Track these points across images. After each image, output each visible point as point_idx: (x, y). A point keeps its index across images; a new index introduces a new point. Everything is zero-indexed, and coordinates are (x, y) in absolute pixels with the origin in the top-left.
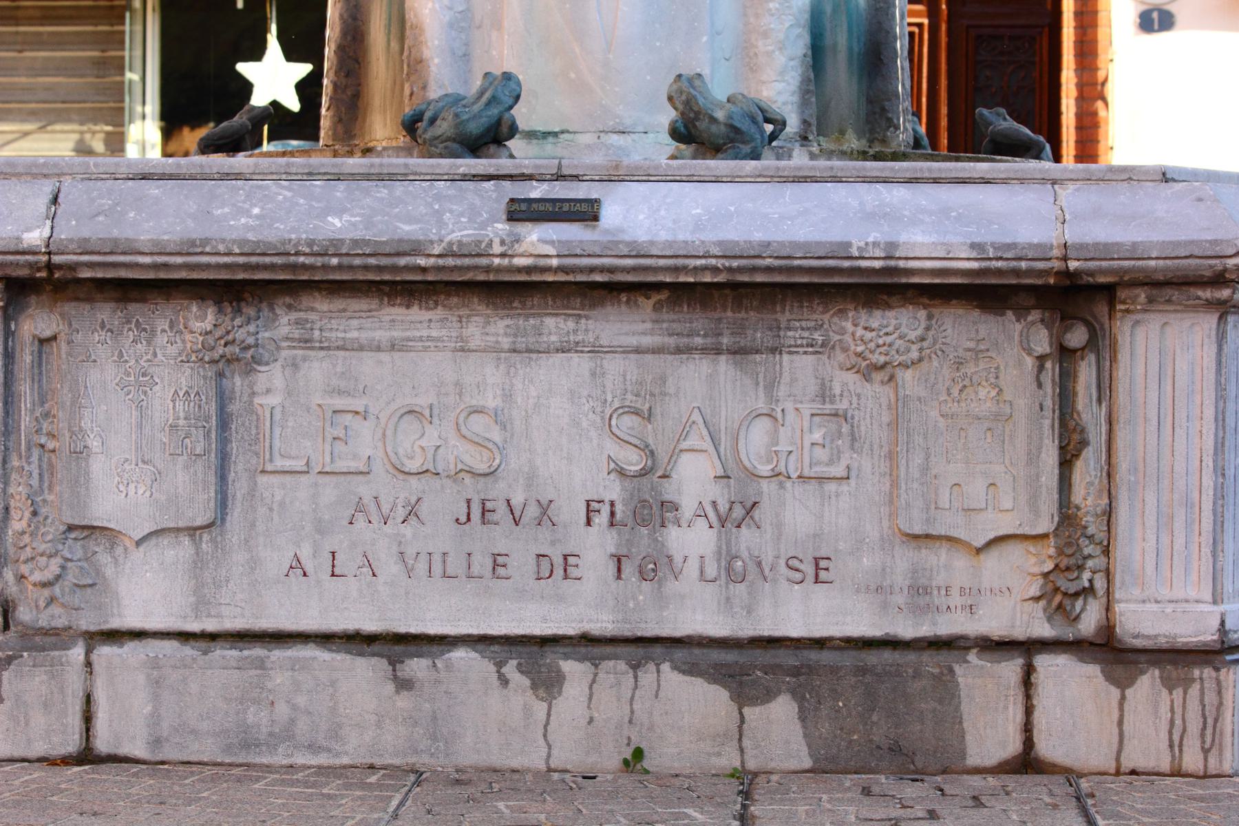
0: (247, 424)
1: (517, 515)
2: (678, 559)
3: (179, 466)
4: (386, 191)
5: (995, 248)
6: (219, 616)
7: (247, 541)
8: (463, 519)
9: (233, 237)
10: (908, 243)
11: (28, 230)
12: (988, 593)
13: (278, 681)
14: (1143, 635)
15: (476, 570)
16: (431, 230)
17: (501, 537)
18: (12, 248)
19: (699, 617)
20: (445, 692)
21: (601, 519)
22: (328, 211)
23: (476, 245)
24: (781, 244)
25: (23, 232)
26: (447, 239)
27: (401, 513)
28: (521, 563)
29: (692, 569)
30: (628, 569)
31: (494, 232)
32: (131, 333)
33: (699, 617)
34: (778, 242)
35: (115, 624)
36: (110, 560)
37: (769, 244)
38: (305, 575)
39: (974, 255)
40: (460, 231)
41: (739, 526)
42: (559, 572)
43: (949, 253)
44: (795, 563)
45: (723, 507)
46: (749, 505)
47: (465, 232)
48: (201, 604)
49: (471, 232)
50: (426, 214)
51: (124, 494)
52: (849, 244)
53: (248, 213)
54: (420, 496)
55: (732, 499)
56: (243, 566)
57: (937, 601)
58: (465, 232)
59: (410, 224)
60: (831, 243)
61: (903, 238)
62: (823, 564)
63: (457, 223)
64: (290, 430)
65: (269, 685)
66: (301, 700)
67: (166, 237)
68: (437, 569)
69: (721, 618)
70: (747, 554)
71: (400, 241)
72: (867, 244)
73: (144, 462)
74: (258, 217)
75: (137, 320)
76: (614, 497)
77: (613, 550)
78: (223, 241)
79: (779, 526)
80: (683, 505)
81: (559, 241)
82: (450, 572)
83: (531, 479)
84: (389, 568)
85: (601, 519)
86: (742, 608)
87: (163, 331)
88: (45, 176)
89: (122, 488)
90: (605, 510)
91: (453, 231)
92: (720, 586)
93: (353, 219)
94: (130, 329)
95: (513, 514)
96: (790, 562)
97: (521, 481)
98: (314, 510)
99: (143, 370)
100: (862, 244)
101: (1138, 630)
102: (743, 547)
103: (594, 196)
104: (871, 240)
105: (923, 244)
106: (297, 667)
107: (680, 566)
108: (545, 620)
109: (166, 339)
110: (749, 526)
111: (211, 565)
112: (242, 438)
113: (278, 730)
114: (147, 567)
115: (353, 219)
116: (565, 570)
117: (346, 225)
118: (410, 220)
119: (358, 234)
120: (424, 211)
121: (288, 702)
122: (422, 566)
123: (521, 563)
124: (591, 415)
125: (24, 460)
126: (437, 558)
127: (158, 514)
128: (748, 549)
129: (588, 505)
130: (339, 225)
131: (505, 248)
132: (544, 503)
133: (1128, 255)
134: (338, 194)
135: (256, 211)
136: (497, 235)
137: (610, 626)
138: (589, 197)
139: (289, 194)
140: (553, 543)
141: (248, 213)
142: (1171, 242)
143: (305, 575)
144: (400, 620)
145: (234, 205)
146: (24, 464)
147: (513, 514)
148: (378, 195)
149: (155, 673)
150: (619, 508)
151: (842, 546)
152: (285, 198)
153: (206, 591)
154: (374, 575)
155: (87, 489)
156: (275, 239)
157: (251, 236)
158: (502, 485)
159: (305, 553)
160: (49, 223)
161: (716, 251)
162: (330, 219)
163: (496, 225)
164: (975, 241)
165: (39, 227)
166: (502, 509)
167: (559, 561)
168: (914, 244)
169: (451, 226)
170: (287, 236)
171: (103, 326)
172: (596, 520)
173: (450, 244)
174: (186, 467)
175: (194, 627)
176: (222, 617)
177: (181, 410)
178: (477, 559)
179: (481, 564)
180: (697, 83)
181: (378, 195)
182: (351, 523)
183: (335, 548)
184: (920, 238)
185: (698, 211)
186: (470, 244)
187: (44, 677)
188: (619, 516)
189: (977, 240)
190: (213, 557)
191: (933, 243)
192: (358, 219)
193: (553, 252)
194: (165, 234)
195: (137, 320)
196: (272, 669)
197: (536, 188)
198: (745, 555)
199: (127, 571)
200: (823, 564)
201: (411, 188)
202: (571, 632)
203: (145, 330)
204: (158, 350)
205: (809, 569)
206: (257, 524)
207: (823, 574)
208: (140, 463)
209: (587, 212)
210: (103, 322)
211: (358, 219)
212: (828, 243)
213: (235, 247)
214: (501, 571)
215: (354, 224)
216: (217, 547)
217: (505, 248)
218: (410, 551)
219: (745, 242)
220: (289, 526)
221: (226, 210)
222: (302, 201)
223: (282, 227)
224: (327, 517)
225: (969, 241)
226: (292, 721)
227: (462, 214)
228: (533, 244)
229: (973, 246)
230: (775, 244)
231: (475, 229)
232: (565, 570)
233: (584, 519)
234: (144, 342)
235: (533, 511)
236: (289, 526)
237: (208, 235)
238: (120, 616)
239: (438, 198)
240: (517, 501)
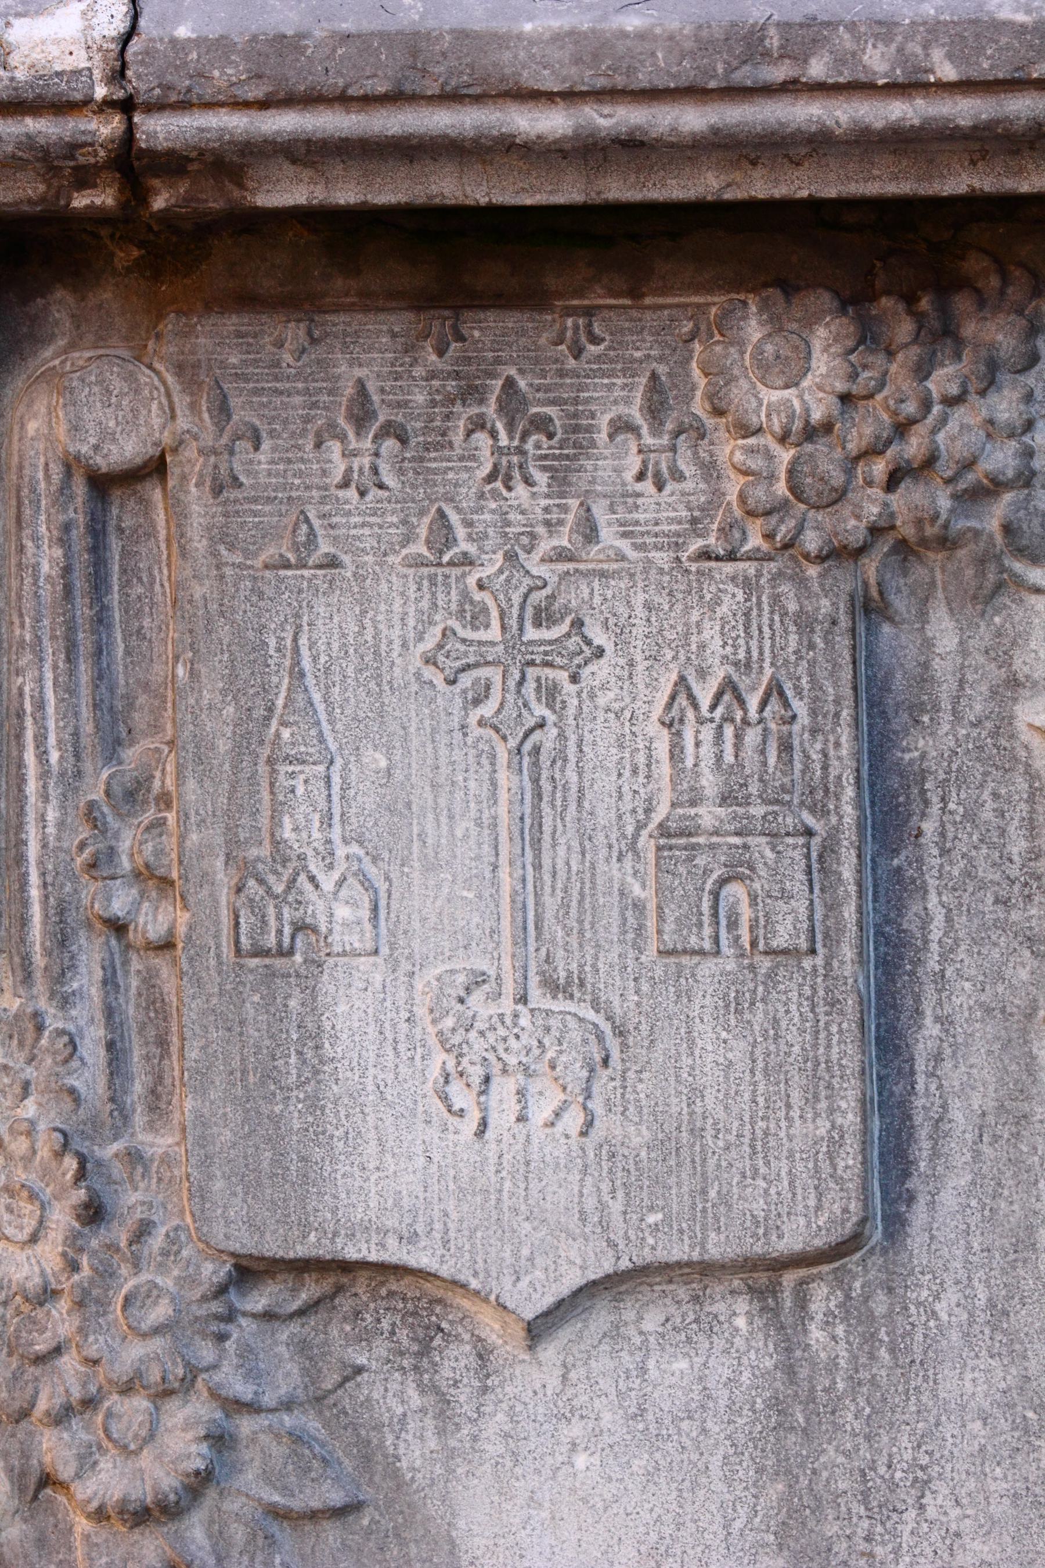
0: (987, 814)
32: (482, 439)
36: (416, 1400)
51: (471, 1124)
75: (510, 384)
87: (622, 426)
94: (479, 424)
109: (634, 463)
153: (832, 1529)
155: (314, 1104)
190: (855, 1384)
199: (494, 1448)
204: (600, 511)
213: (937, 55)
234: (541, 478)
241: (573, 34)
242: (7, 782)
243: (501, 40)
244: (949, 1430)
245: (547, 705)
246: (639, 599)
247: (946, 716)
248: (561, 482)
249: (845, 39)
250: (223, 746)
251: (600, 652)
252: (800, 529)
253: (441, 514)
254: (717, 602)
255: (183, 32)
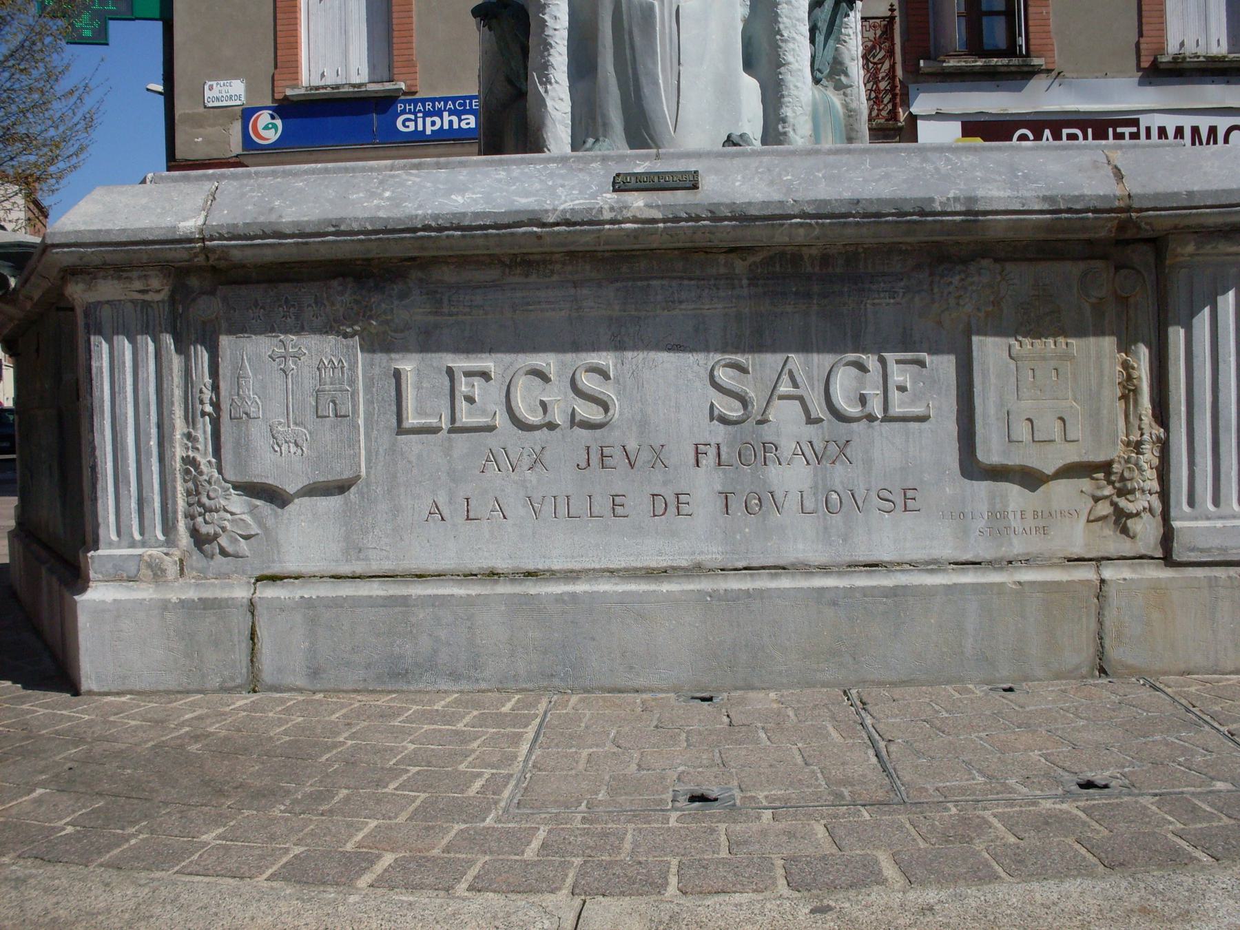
0: (386, 387)
1: (632, 458)
2: (779, 495)
3: (327, 426)
4: (504, 173)
5: (1064, 199)
6: (367, 559)
7: (389, 491)
8: (583, 464)
9: (366, 216)
10: (986, 197)
11: (184, 220)
12: (1059, 515)
13: (421, 616)
14: (1198, 548)
15: (596, 510)
16: (545, 202)
17: (618, 480)
18: (170, 236)
19: (800, 546)
20: (572, 622)
21: (709, 460)
22: (449, 192)
23: (587, 212)
24: (870, 201)
25: (180, 222)
26: (562, 207)
27: (526, 461)
28: (638, 503)
29: (792, 504)
30: (736, 505)
31: (603, 201)
32: (281, 309)
33: (800, 546)
34: (866, 200)
35: (275, 569)
36: (270, 512)
37: (858, 201)
38: (443, 519)
39: (1046, 207)
40: (572, 201)
41: (833, 463)
42: (672, 509)
43: (1023, 205)
44: (885, 494)
45: (819, 446)
46: (841, 442)
47: (577, 202)
48: (354, 549)
49: (582, 201)
50: (541, 189)
51: (279, 454)
52: (932, 200)
53: (380, 197)
54: (544, 445)
55: (827, 439)
56: (386, 513)
57: (1013, 524)
58: (577, 202)
59: (527, 197)
60: (915, 200)
61: (980, 193)
62: (910, 494)
63: (569, 195)
64: (424, 391)
65: (413, 620)
66: (443, 634)
67: (306, 219)
68: (563, 510)
69: (820, 546)
70: (841, 487)
71: (517, 212)
72: (948, 199)
73: (295, 424)
74: (388, 199)
75: (286, 298)
76: (719, 440)
77: (720, 488)
78: (356, 219)
79: (868, 462)
80: (782, 446)
81: (664, 205)
82: (1071, 436)
83: (643, 425)
84: (515, 509)
85: (709, 460)
86: (839, 537)
87: (309, 305)
88: (763, 689)
89: (277, 448)
90: (712, 452)
91: (566, 202)
92: (818, 517)
93: (474, 196)
94: (280, 306)
95: (628, 458)
96: (882, 494)
97: (634, 428)
98: (449, 462)
99: (293, 342)
100: (944, 199)
101: (1193, 544)
102: (837, 481)
103: (693, 169)
104: (951, 195)
105: (1000, 198)
106: (437, 604)
107: (782, 500)
108: (660, 554)
109: (312, 313)
110: (843, 463)
111: (358, 514)
112: (383, 399)
113: (422, 661)
114: (302, 517)
115: (474, 196)
116: (678, 508)
117: (468, 201)
118: (527, 194)
119: (479, 208)
120: (538, 187)
121: (431, 635)
122: (548, 508)
123: (638, 503)
124: (696, 368)
125: (191, 427)
126: (562, 502)
127: (309, 470)
128: (842, 483)
129: (697, 448)
130: (462, 201)
131: (614, 214)
132: (657, 447)
133: (1185, 204)
134: (461, 177)
135: (387, 194)
136: (606, 202)
137: (720, 557)
138: (688, 170)
139: (418, 180)
140: (665, 483)
141: (380, 197)
142: (1224, 191)
143: (443, 519)
144: (528, 558)
145: (367, 191)
146: (191, 430)
147: (628, 458)
148: (497, 176)
149: (311, 612)
150: (724, 450)
151: (926, 477)
152: (414, 182)
153: (355, 537)
154: (505, 518)
155: (247, 450)
156: (403, 215)
157: (382, 214)
158: (617, 433)
159: (441, 501)
160: (204, 213)
161: (810, 209)
162: (453, 197)
163: (604, 195)
164: (1047, 194)
165: (194, 217)
166: (618, 453)
167: (671, 500)
168: (991, 199)
169: (563, 198)
170: (414, 212)
171: (256, 304)
172: (703, 462)
173: (564, 211)
174: (333, 427)
175: (345, 569)
176: (369, 560)
177: (327, 376)
178: (597, 499)
179: (602, 505)
180: (745, 138)
181: (497, 176)
182: (483, 472)
183: (469, 495)
184: (995, 193)
185: (789, 177)
186: (582, 212)
187: (214, 619)
188: (723, 457)
189: (1048, 193)
190: (360, 507)
191: (1009, 197)
192: (478, 196)
193: (659, 215)
194: (304, 216)
195: (286, 298)
196: (414, 606)
197: (639, 165)
198: (839, 488)
199: (285, 521)
200: (910, 494)
201: (526, 170)
202: (684, 564)
203: (293, 306)
204: (305, 324)
205: (899, 501)
206: (399, 475)
207: (619, 510)
208: (292, 426)
209: (690, 182)
210: (256, 301)
211: (478, 196)
212: (911, 199)
213: (367, 224)
214: (619, 510)
215: (475, 200)
216: (363, 497)
217: (614, 214)
218: (537, 496)
219: (836, 200)
220: (427, 477)
221: (361, 195)
222: (429, 185)
223: (410, 205)
224: (460, 467)
225: (1041, 195)
226: (435, 651)
227: (573, 188)
228: (638, 208)
229: (1045, 199)
230: (864, 202)
231: (586, 199)
232: (678, 508)
233: (693, 461)
234: (293, 317)
235: (645, 456)
236: (427, 477)
237: (343, 214)
238: (280, 562)
239: (551, 175)
240: (632, 446)
241: (293, 221)
242: (181, 323)
243: (278, 223)
244: (379, 516)
245: (526, 726)
246: (313, 342)
247: (378, 367)
248: (297, 318)
249: (348, 221)
250: (229, 375)
251: (305, 354)
252: (773, 701)
253: (273, 325)
254: (329, 342)
255: (214, 224)
